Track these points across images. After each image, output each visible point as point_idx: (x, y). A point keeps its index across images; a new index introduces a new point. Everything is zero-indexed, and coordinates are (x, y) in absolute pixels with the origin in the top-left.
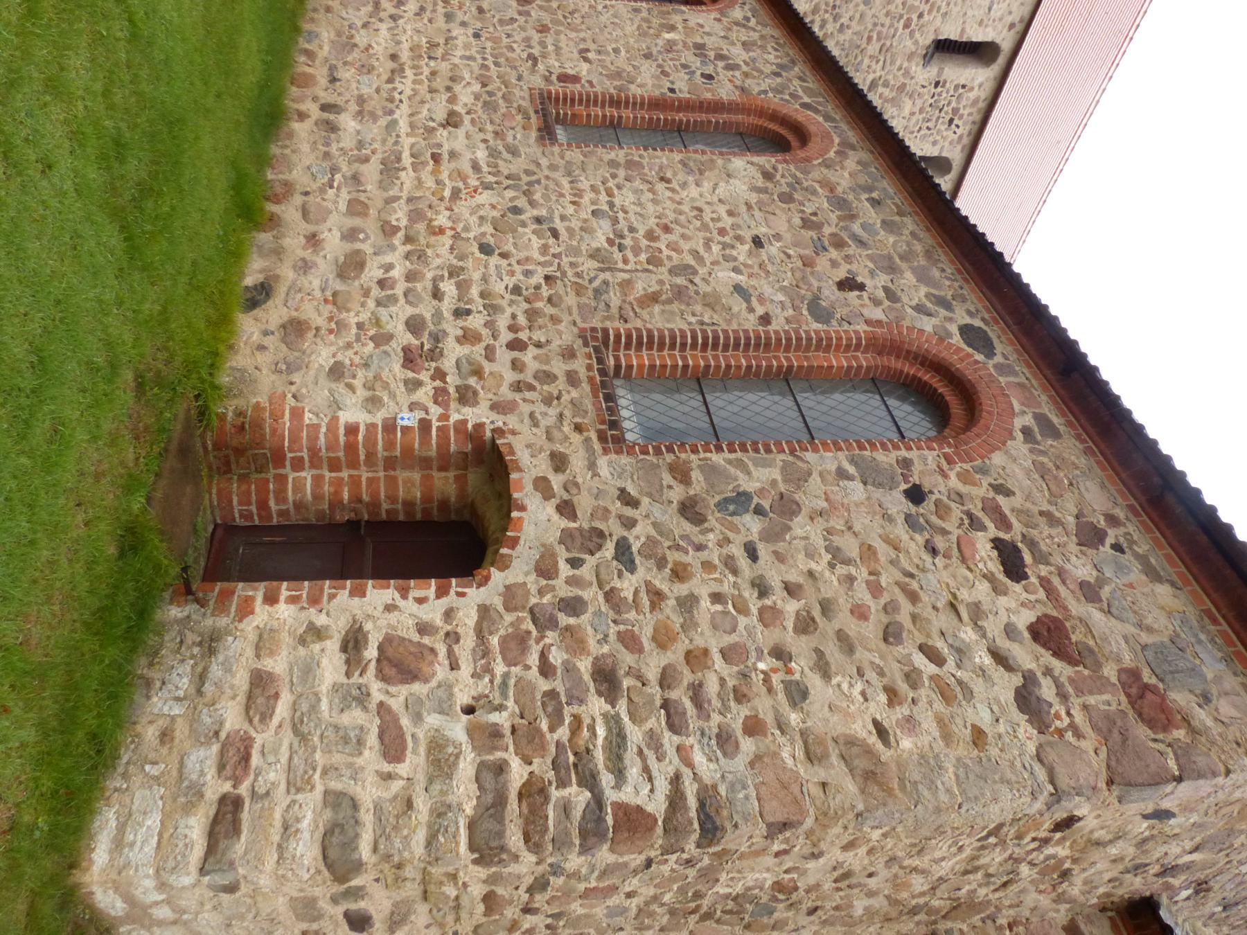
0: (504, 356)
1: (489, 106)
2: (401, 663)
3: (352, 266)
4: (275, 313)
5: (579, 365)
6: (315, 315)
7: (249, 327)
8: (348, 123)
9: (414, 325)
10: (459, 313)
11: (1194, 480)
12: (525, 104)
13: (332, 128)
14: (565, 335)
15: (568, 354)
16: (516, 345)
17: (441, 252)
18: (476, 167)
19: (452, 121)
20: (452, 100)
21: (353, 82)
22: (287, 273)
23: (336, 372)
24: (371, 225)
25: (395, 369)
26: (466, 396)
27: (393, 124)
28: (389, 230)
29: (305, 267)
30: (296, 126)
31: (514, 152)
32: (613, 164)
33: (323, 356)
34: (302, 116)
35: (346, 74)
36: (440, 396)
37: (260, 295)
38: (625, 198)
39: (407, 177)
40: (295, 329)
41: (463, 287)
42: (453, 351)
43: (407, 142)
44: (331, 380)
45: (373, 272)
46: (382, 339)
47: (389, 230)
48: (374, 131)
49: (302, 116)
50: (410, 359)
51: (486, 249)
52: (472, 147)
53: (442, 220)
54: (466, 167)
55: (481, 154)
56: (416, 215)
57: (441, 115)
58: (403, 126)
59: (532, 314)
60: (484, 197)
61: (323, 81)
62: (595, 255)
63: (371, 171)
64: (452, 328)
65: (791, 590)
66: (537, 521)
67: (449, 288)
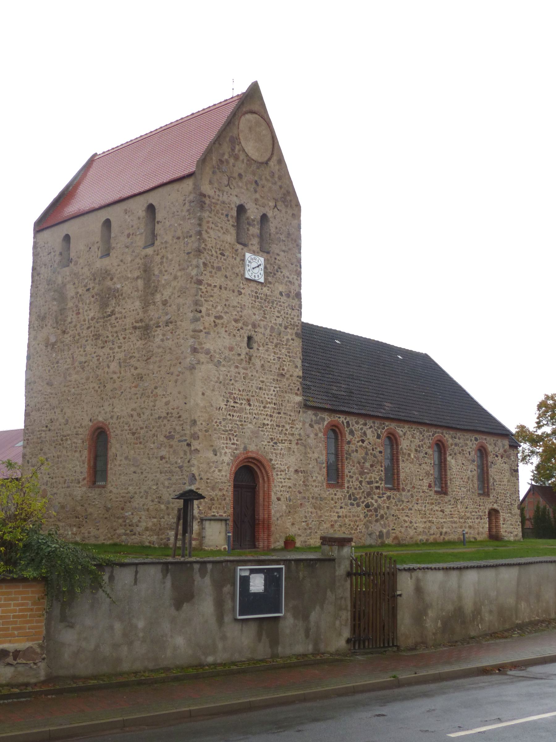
0: (481, 507)
1: (439, 503)
2: (504, 520)
3: (470, 527)
4: (477, 536)
5: (482, 498)
6: (476, 531)
7: (479, 539)
8: (444, 530)
9: (477, 518)
10: (476, 512)
11: (391, 344)
12: (438, 496)
13: (446, 533)
14: (478, 498)
15: (480, 499)
16: (480, 506)
17: (468, 515)
18: (453, 508)
19: (442, 511)
20: (437, 511)
21: (434, 529)
22: (472, 536)
23: (483, 528)
24: (464, 525)
25: (483, 521)
26: (485, 512)
27: (444, 522)
28: (465, 522)
29: (470, 533)
30: (446, 539)
31: (450, 501)
32: (450, 483)
33: (481, 529)
34: (444, 539)
35: (432, 532)
36: (485, 515)
37: (475, 538)
38: (457, 483)
39: (455, 519)
40: (478, 534)
41: (473, 512)
42: (480, 514)
43: (448, 520)
44: (482, 528)
45: (471, 524)
46: (479, 523)
47: (465, 522)
48: (445, 525)
49: (444, 539)
50: (481, 519)
51: (467, 508)
52: (448, 508)
53: (463, 514)
54: (452, 509)
55: (450, 507)
56: (462, 518)
57: (441, 513)
58: (445, 520)
59: (476, 503)
60: (459, 506)
61: (434, 536)
62: (467, 491)
63: (454, 525)
64: (478, 514)
65: (231, 380)
66: (495, 506)
67: (473, 514)
